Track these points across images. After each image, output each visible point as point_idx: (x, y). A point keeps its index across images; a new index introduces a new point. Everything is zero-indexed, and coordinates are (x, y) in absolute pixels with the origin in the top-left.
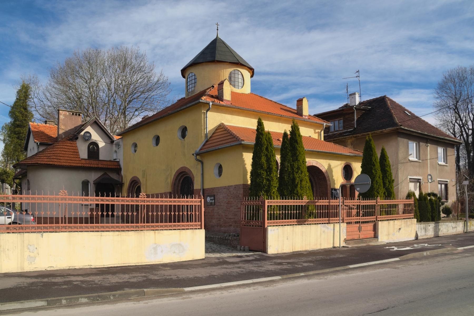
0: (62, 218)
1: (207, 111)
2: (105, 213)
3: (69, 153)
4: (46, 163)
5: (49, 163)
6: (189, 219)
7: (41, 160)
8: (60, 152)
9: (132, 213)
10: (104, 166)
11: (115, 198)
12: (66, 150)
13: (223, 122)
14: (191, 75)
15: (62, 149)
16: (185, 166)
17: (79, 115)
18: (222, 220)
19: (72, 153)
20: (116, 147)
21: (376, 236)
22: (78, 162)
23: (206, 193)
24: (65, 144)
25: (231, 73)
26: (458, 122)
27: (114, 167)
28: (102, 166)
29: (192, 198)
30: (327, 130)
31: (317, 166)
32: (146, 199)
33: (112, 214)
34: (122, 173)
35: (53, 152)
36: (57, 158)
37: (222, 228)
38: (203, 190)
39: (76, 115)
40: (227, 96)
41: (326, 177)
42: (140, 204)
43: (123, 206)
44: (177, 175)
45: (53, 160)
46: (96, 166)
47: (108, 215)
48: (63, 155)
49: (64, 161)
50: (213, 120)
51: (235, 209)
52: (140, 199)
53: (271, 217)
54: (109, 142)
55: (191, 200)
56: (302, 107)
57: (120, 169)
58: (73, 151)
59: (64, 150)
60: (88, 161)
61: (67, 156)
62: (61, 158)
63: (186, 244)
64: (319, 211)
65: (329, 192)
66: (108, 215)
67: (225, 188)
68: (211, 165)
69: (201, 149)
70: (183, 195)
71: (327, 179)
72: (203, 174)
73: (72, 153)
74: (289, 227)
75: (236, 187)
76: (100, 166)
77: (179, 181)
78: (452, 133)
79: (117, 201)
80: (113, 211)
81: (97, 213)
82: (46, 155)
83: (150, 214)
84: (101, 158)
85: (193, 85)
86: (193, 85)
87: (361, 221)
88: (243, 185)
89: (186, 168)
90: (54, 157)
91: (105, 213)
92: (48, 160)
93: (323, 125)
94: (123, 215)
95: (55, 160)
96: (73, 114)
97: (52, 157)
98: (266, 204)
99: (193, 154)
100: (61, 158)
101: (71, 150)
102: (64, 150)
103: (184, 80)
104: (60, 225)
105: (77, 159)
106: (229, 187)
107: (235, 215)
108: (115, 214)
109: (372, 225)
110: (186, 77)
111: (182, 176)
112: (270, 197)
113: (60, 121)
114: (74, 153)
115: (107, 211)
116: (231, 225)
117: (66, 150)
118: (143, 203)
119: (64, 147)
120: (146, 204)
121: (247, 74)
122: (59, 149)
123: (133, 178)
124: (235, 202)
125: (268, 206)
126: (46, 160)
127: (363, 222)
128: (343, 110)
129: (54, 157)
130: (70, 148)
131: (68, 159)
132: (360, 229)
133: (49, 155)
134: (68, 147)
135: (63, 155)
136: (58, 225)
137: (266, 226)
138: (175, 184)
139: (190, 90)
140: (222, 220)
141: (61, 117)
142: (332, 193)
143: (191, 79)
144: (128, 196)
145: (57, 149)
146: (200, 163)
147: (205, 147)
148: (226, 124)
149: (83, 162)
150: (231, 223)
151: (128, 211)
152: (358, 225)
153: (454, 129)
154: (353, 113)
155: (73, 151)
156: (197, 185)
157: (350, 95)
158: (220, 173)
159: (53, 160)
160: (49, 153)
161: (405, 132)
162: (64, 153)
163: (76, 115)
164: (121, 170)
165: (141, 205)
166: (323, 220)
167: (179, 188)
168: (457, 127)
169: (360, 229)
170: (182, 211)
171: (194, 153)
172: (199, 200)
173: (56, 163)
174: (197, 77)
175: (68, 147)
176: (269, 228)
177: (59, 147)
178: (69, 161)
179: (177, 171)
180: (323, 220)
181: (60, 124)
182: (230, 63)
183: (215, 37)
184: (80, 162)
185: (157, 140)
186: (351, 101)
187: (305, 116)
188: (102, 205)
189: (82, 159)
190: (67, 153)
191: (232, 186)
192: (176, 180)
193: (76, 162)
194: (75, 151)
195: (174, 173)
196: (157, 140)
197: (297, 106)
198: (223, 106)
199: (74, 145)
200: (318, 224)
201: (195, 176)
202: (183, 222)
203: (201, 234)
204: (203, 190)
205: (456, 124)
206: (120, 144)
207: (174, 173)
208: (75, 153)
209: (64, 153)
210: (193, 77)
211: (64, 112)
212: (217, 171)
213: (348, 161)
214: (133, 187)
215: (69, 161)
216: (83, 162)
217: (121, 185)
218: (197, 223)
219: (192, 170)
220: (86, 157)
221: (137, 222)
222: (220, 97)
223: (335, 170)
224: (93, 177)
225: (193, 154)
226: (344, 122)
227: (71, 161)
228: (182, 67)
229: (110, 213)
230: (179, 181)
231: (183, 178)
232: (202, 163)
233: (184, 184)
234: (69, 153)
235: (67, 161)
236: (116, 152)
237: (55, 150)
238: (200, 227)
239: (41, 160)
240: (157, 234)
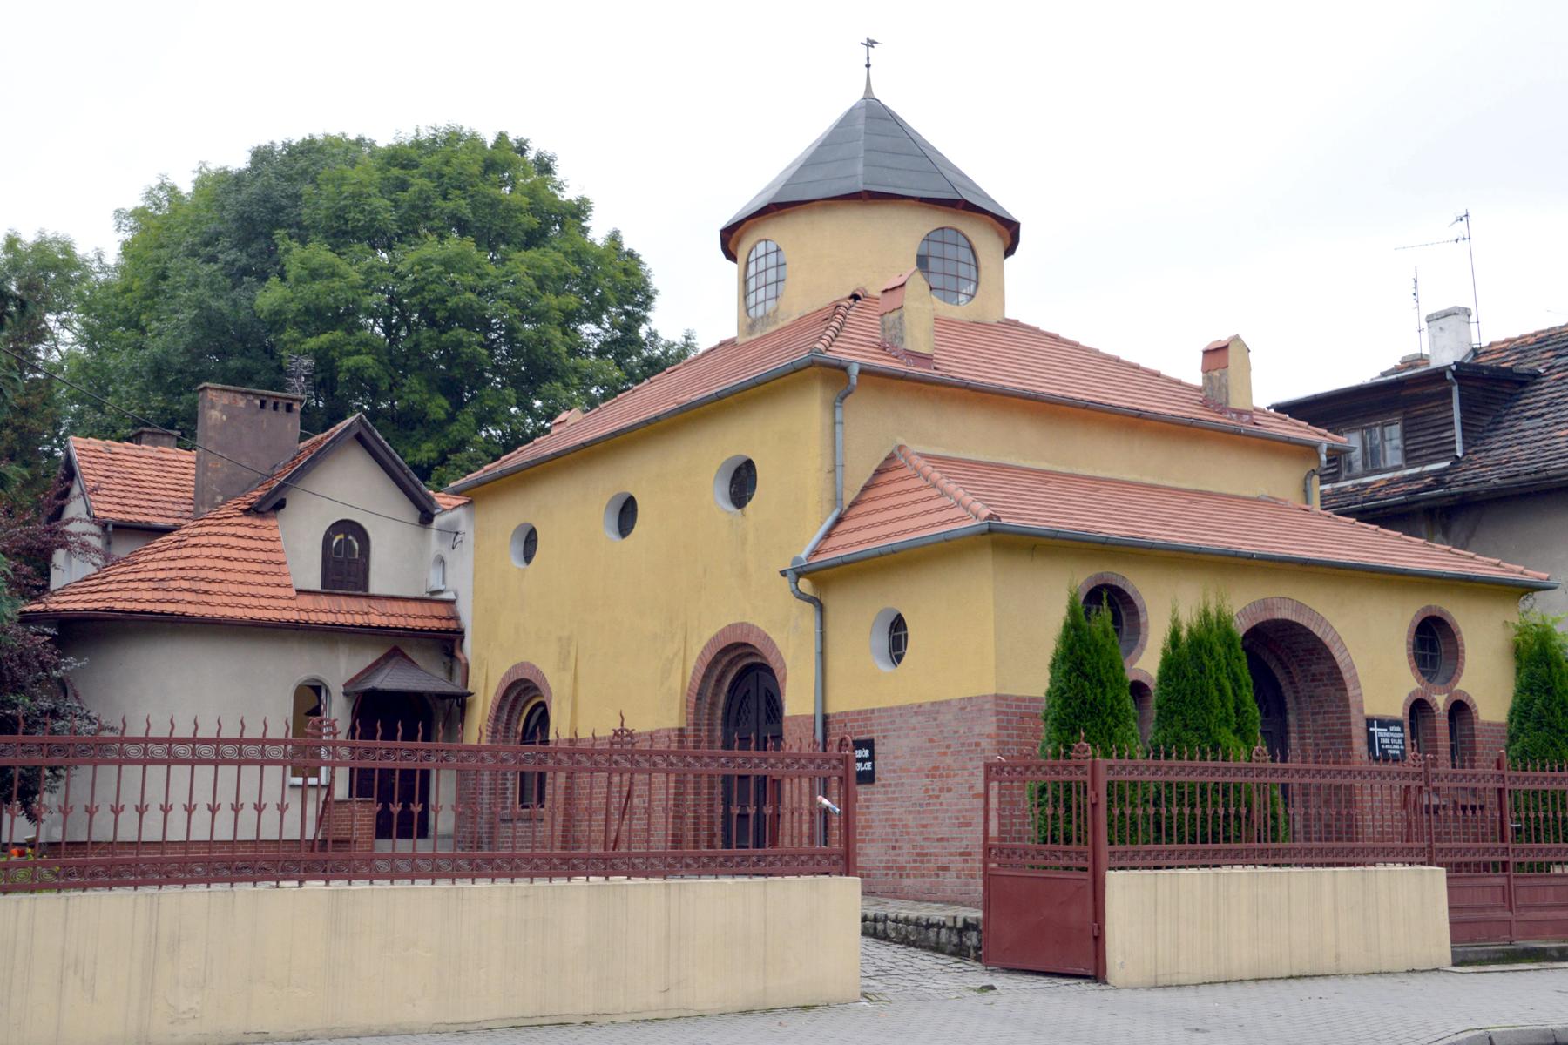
3: (248, 566)
4: (149, 607)
5: (159, 607)
8: (210, 563)
12: (234, 554)
14: (761, 249)
15: (216, 552)
16: (746, 620)
17: (289, 408)
18: (907, 847)
19: (257, 567)
22: (284, 603)
27: (436, 624)
28: (384, 621)
31: (1301, 620)
36: (197, 586)
37: (906, 881)
39: (275, 407)
41: (1342, 666)
44: (709, 657)
45: (178, 596)
46: (359, 620)
48: (220, 576)
49: (226, 600)
51: (961, 797)
53: (1124, 831)
54: (416, 521)
57: (459, 634)
58: (263, 556)
60: (325, 603)
61: (240, 577)
62: (214, 587)
65: (1358, 731)
67: (918, 710)
68: (858, 620)
69: (815, 552)
71: (1346, 676)
73: (257, 567)
75: (968, 706)
76: (375, 620)
77: (719, 681)
82: (151, 575)
84: (375, 587)
85: (772, 290)
86: (772, 290)
88: (997, 697)
89: (751, 627)
92: (160, 595)
95: (188, 596)
96: (263, 404)
97: (173, 584)
98: (1103, 779)
99: (783, 573)
100: (214, 587)
101: (253, 555)
103: (732, 269)
107: (960, 825)
110: (741, 256)
111: (731, 663)
116: (945, 869)
117: (234, 554)
119: (224, 540)
122: (206, 551)
124: (964, 768)
125: (1110, 784)
129: (185, 584)
131: (244, 589)
132: (1507, 894)
134: (243, 543)
135: (220, 576)
138: (699, 697)
139: (760, 310)
140: (907, 847)
142: (1371, 736)
143: (762, 267)
145: (195, 551)
146: (810, 607)
147: (833, 542)
150: (943, 861)
154: (1449, 394)
155: (263, 556)
159: (178, 596)
162: (228, 565)
163: (275, 407)
164: (462, 640)
167: (720, 713)
170: (757, 803)
171: (787, 566)
173: (191, 610)
174: (787, 256)
175: (243, 543)
178: (245, 601)
179: (714, 639)
183: (857, 95)
184: (293, 604)
186: (1432, 343)
189: (299, 592)
190: (237, 565)
191: (948, 703)
192: (706, 676)
193: (274, 603)
194: (273, 557)
196: (627, 514)
197: (1206, 370)
204: (825, 718)
206: (461, 529)
208: (273, 568)
209: (228, 565)
210: (772, 259)
211: (225, 399)
212: (884, 642)
214: (513, 707)
215: (245, 601)
216: (307, 602)
220: (316, 585)
224: (340, 669)
225: (783, 573)
226: (1406, 435)
227: (254, 602)
228: (723, 223)
230: (719, 681)
231: (740, 665)
232: (821, 608)
234: (248, 566)
235: (236, 600)
236: (441, 561)
237: (186, 552)
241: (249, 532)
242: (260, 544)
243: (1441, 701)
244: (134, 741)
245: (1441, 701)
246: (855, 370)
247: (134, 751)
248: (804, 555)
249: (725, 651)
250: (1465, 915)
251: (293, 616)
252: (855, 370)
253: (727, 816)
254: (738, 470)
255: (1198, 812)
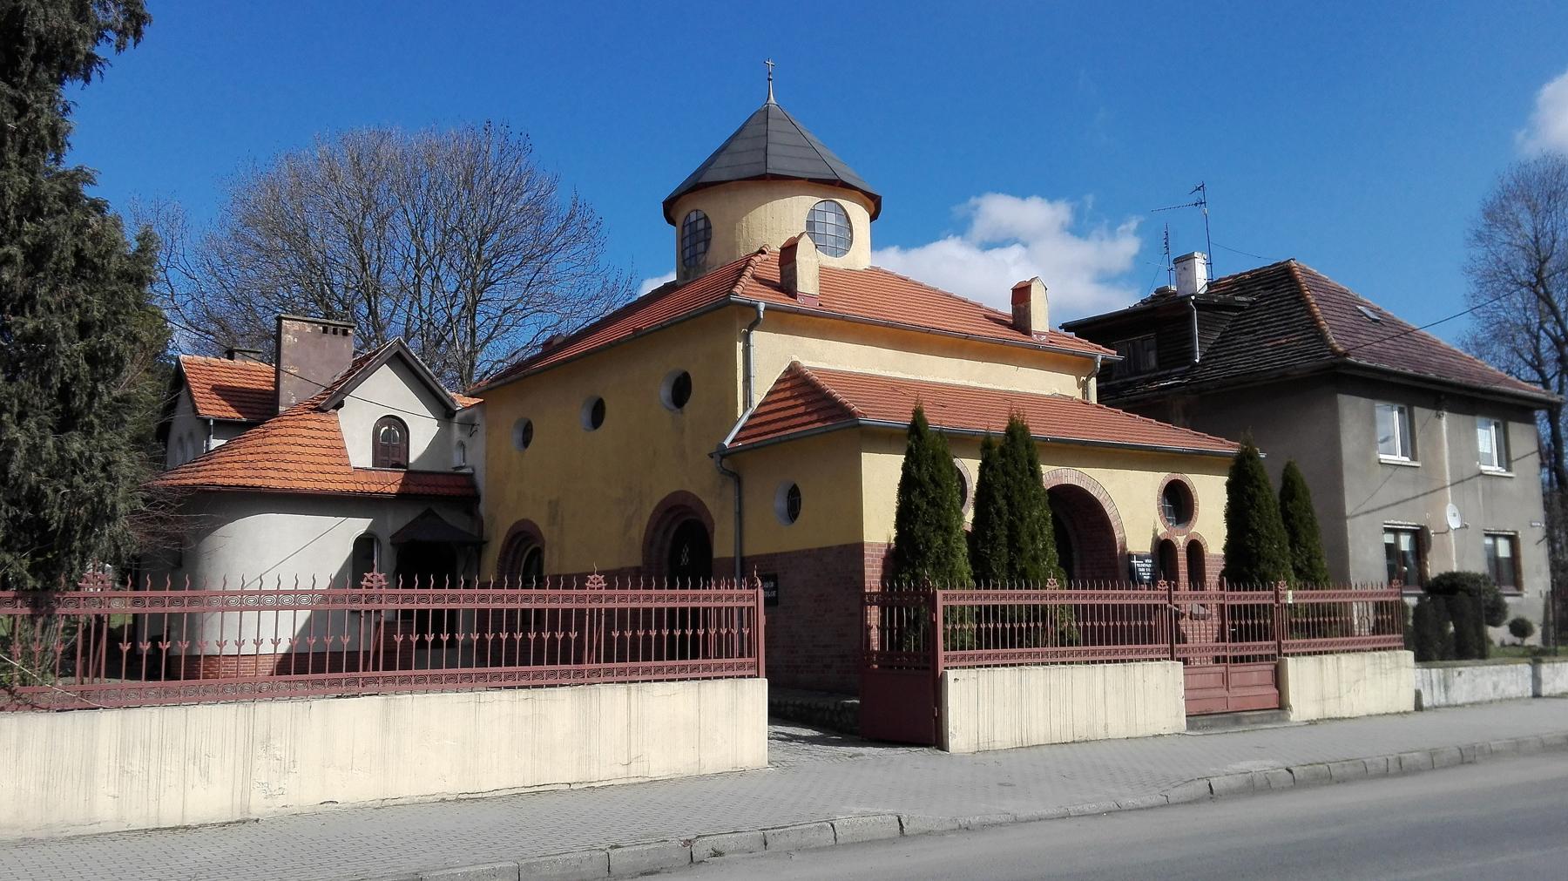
0: (367, 653)
1: (751, 329)
2: (430, 638)
3: (315, 451)
4: (242, 482)
5: (250, 482)
6: (724, 649)
7: (223, 473)
9: (511, 635)
10: (427, 490)
11: (462, 591)
12: (306, 441)
13: (796, 358)
17: (345, 333)
19: (324, 451)
20: (462, 430)
21: (1282, 705)
22: (343, 478)
23: (767, 570)
24: (303, 424)
25: (813, 210)
26: (1547, 326)
28: (420, 490)
29: (718, 588)
30: (1106, 374)
32: (603, 591)
33: (437, 638)
34: (483, 508)
35: (266, 449)
38: (743, 559)
39: (335, 332)
40: (807, 282)
42: (587, 606)
43: (483, 613)
47: (422, 644)
49: (301, 476)
50: (769, 357)
52: (587, 592)
53: (955, 643)
55: (729, 591)
56: (1028, 307)
57: (476, 498)
58: (328, 443)
59: (300, 441)
60: (375, 476)
62: (291, 466)
63: (708, 727)
64: (560, 636)
66: (437, 643)
67: (808, 554)
70: (707, 578)
71: (1114, 524)
72: (740, 515)
73: (324, 451)
74: (1007, 669)
78: (1531, 364)
79: (462, 599)
80: (452, 630)
81: (497, 636)
83: (616, 634)
87: (1229, 654)
88: (862, 544)
90: (269, 464)
91: (430, 638)
92: (250, 473)
93: (1093, 358)
94: (482, 642)
96: (325, 330)
97: (260, 465)
98: (940, 603)
99: (711, 456)
100: (291, 466)
102: (300, 441)
104: (361, 673)
105: (341, 469)
106: (823, 551)
108: (460, 637)
109: (1268, 667)
110: (680, 220)
112: (949, 578)
113: (284, 351)
114: (329, 451)
115: (438, 630)
117: (306, 441)
118: (595, 605)
120: (604, 605)
121: (859, 214)
123: (517, 523)
126: (241, 473)
127: (1235, 660)
128: (1153, 309)
129: (269, 464)
130: (319, 434)
131: (313, 468)
132: (1225, 679)
133: (250, 458)
134: (312, 433)
135: (295, 457)
136: (354, 674)
137: (941, 669)
141: (288, 339)
144: (499, 585)
148: (806, 363)
149: (362, 477)
151: (497, 629)
152: (1220, 668)
153: (1537, 349)
154: (1190, 316)
155: (328, 443)
156: (723, 547)
157: (1177, 261)
158: (793, 510)
160: (251, 450)
161: (1360, 373)
162: (300, 449)
165: (591, 610)
166: (1109, 652)
168: (1545, 343)
169: (1225, 679)
170: (705, 626)
172: (751, 592)
175: (312, 433)
176: (951, 675)
177: (283, 431)
178: (315, 476)
179: (663, 502)
180: (1109, 652)
181: (284, 361)
182: (810, 180)
184: (350, 478)
185: (598, 414)
187: (1039, 334)
188: (423, 614)
190: (308, 450)
194: (335, 443)
195: (650, 511)
196: (598, 414)
198: (798, 312)
199: (330, 426)
200: (1094, 662)
201: (715, 518)
202: (706, 656)
203: (756, 692)
204: (743, 559)
205: (1542, 333)
206: (477, 421)
207: (648, 510)
208: (337, 452)
211: (297, 326)
213: (1178, 476)
215: (315, 476)
216: (362, 477)
217: (478, 546)
218: (746, 660)
219: (708, 502)
220: (370, 466)
221: (579, 661)
222: (787, 285)
223: (1132, 504)
225: (711, 456)
227: (322, 477)
229: (445, 637)
232: (739, 481)
233: (681, 544)
234: (315, 451)
238: (753, 672)
239: (223, 473)
240: (633, 693)
241: (318, 425)
242: (326, 434)
243: (1181, 541)
244: (234, 594)
245: (1181, 541)
246: (762, 306)
247: (233, 601)
248: (727, 443)
249: (669, 510)
250: (1197, 694)
251: (351, 487)
252: (762, 306)
253: (609, 640)
254: (678, 380)
255: (1024, 626)
